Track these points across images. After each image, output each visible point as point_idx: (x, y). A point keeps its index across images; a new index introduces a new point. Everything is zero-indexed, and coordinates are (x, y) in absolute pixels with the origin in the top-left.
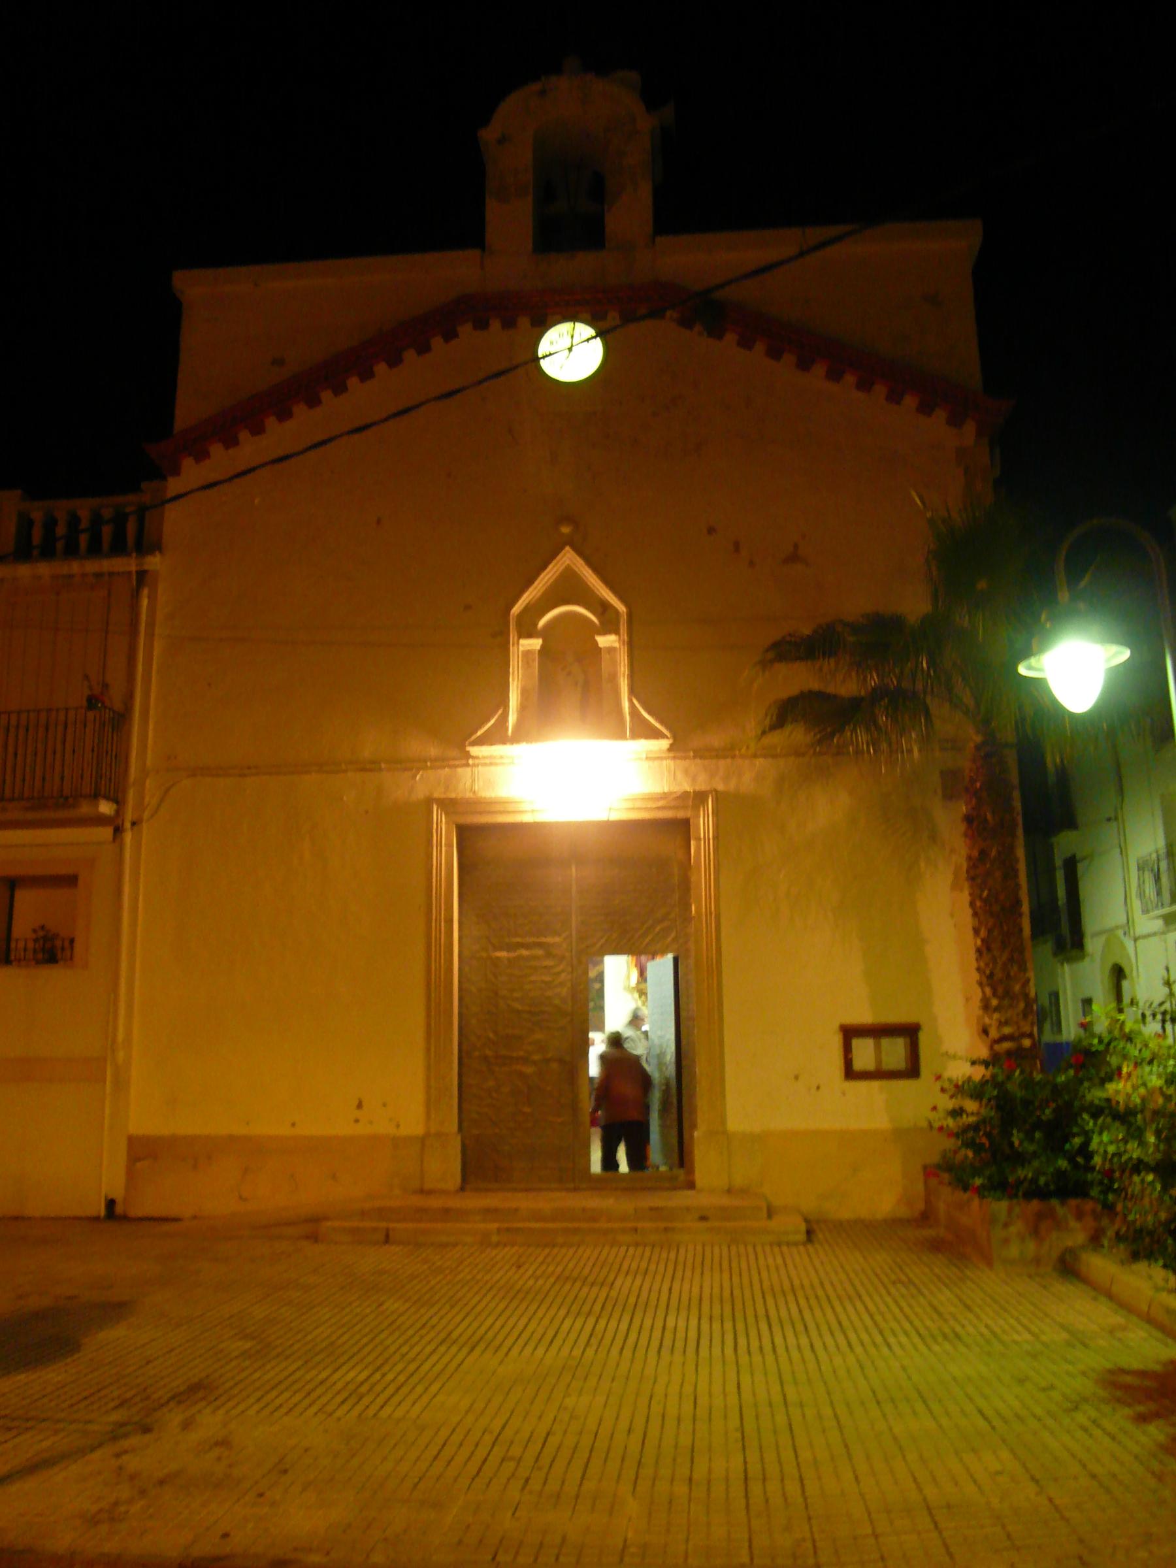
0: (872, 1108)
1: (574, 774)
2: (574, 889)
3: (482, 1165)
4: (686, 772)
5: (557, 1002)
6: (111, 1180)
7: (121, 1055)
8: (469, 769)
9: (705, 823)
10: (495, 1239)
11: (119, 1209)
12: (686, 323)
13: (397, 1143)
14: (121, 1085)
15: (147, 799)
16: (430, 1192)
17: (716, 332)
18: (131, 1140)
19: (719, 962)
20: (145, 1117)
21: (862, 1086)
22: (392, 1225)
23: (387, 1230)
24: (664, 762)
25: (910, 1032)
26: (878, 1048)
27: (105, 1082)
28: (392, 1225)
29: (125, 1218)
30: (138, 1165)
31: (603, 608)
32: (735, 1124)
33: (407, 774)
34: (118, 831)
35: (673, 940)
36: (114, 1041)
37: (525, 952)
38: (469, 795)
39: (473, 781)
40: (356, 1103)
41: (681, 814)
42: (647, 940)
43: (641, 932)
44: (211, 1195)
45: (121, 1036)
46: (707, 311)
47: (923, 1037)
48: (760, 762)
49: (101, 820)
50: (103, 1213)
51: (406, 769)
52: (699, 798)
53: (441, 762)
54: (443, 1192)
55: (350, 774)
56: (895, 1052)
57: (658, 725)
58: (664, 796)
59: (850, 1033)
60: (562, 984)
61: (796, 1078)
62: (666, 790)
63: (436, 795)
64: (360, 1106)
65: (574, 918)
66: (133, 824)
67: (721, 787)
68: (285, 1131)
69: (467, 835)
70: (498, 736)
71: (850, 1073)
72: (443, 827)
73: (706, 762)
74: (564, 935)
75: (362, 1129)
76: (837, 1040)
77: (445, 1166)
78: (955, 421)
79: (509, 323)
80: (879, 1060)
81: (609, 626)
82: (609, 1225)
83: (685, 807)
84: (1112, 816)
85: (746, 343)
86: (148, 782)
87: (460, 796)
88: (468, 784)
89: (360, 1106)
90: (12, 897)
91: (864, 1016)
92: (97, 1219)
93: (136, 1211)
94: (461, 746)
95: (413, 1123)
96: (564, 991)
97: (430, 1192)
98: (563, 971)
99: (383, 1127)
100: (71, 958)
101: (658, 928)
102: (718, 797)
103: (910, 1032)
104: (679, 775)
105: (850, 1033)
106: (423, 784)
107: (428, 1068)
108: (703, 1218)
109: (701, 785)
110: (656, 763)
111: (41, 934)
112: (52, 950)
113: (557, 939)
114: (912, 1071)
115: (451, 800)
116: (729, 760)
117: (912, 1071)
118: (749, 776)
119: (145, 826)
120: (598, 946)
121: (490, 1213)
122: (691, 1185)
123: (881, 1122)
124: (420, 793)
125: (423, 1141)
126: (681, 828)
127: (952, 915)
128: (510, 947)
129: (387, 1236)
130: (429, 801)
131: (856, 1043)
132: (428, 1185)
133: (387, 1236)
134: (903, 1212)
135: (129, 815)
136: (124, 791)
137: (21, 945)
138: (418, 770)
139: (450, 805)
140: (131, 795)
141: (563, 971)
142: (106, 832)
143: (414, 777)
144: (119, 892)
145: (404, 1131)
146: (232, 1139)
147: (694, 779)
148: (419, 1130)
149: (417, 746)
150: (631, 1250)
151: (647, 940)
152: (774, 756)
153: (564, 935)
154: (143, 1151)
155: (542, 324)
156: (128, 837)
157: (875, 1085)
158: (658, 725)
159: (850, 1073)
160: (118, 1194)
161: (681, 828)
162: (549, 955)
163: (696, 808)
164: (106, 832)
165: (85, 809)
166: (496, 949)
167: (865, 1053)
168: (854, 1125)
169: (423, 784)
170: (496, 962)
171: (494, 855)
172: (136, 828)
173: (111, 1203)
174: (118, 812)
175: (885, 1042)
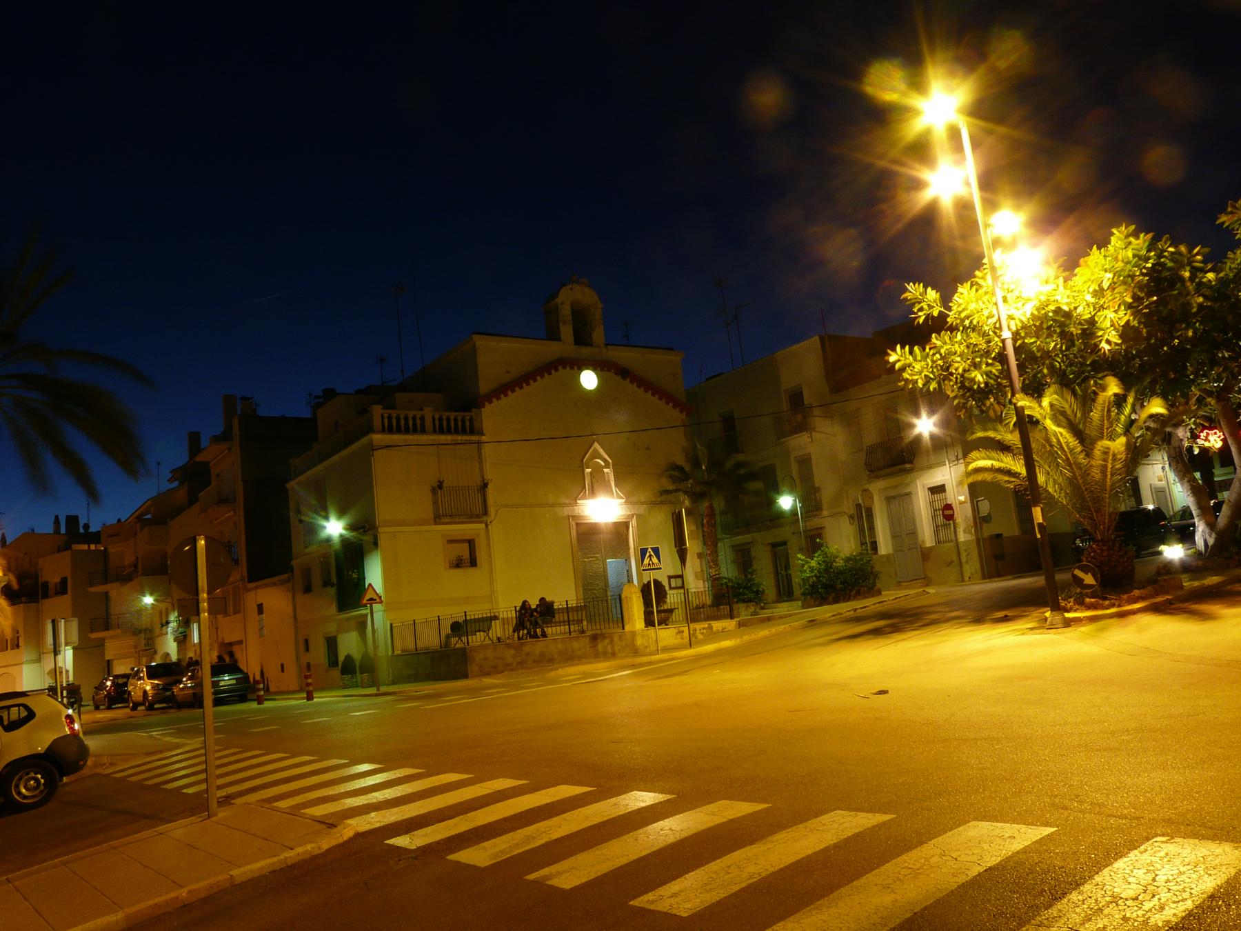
1: (604, 508)
9: (634, 523)
12: (617, 374)
17: (624, 378)
31: (604, 460)
46: (624, 372)
53: (570, 505)
57: (177, 740)
70: (585, 498)
72: (573, 523)
78: (681, 412)
79: (572, 368)
81: (607, 466)
84: (564, 594)
85: (632, 382)
94: (576, 499)
139: (574, 517)
149: (563, 500)
155: (580, 370)
158: (177, 740)
161: (626, 525)
169: (566, 511)
171: (587, 534)
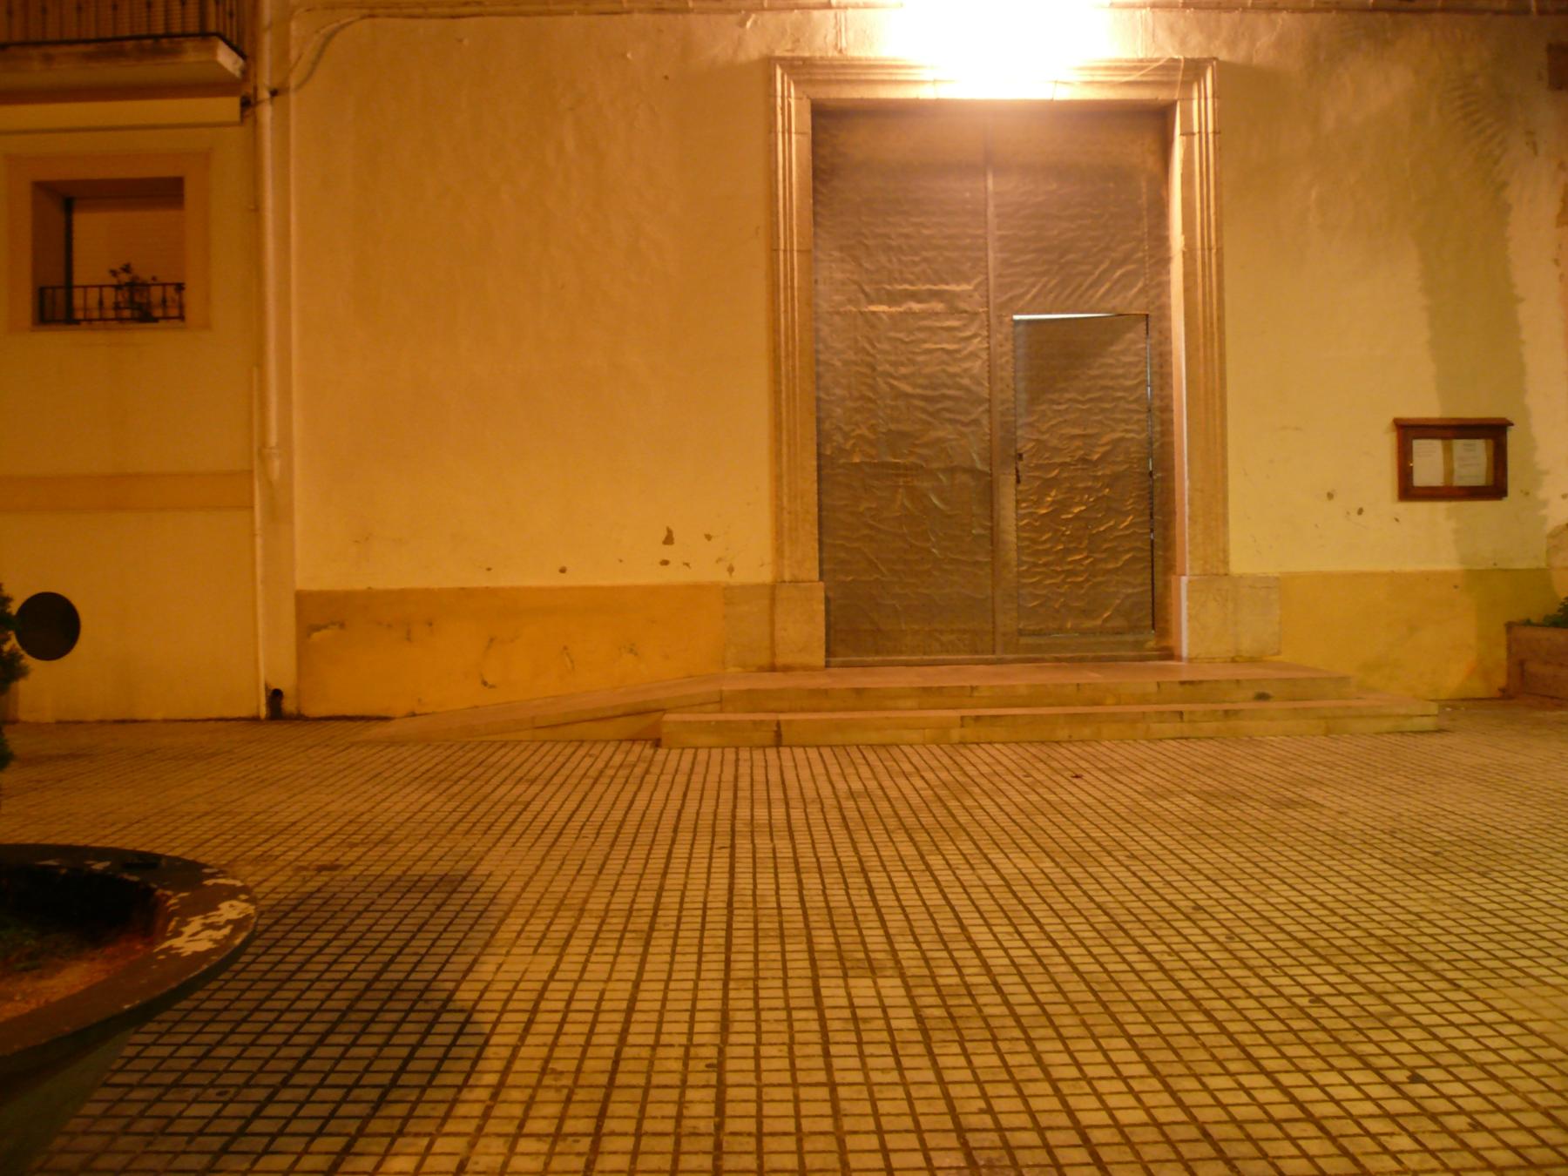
0: (1434, 540)
2: (991, 210)
3: (853, 630)
4: (1172, 30)
5: (966, 381)
6: (275, 661)
7: (276, 464)
8: (830, 13)
9: (1199, 110)
10: (956, 735)
11: (289, 706)
13: (730, 595)
14: (279, 514)
15: (294, 54)
16: (787, 669)
18: (302, 598)
19: (1221, 319)
20: (318, 569)
21: (1422, 508)
22: (782, 717)
23: (778, 724)
24: (1138, 13)
25: (1494, 432)
26: (1448, 451)
27: (252, 507)
28: (782, 717)
29: (300, 718)
30: (316, 636)
32: (1242, 562)
33: (732, 18)
34: (248, 104)
35: (1141, 291)
36: (264, 444)
37: (916, 307)
38: (832, 53)
39: (838, 33)
40: (663, 534)
41: (1162, 95)
42: (1102, 290)
43: (1090, 279)
44: (436, 680)
45: (273, 439)
47: (1511, 435)
48: (1283, 18)
49: (220, 86)
50: (263, 712)
51: (730, 11)
52: (1194, 69)
54: (807, 668)
55: (636, 16)
56: (1472, 460)
58: (1139, 65)
59: (1408, 432)
60: (973, 355)
61: (1330, 496)
62: (1141, 55)
63: (778, 53)
64: (669, 540)
65: (991, 254)
66: (274, 93)
67: (1224, 56)
68: (548, 579)
69: (828, 119)
71: (1408, 491)
73: (1202, 15)
74: (976, 281)
75: (675, 576)
76: (1387, 445)
77: (802, 630)
80: (1449, 472)
82: (1118, 709)
83: (1169, 84)
86: (293, 25)
87: (818, 54)
88: (831, 38)
89: (669, 540)
90: (730, 1171)
91: (1429, 408)
92: (255, 719)
93: (314, 710)
95: (753, 562)
96: (977, 366)
97: (787, 669)
98: (975, 336)
99: (707, 572)
100: (181, 317)
101: (1118, 273)
102: (1225, 72)
103: (1494, 432)
104: (1161, 34)
105: (1408, 432)
106: (758, 36)
107: (777, 479)
108: (1262, 697)
109: (1196, 48)
110: (1126, 13)
111: (125, 278)
112: (144, 303)
113: (965, 287)
114: (1495, 489)
115: (804, 60)
116: (1236, 15)
117: (1495, 489)
118: (1265, 40)
119: (293, 97)
120: (1029, 297)
121: (929, 695)
122: (1169, 654)
123: (1447, 562)
124: (754, 49)
125: (772, 592)
126: (1155, 120)
127: (1556, 262)
128: (893, 299)
129: (778, 734)
130: (769, 63)
131: (1419, 445)
132: (781, 660)
133: (778, 734)
134: (1479, 688)
135: (266, 79)
136: (255, 40)
137: (93, 295)
138: (749, 11)
139: (802, 69)
140: (267, 41)
141: (975, 336)
142: (228, 107)
143: (742, 24)
144: (256, 209)
145: (741, 577)
146: (466, 593)
147: (1183, 43)
148: (766, 576)
150: (716, 753)
151: (1102, 290)
152: (1305, 11)
153: (976, 281)
154: (321, 616)
156: (266, 113)
157: (1442, 506)
159: (1408, 491)
160: (286, 684)
161: (1155, 120)
162: (954, 311)
163: (1186, 85)
164: (228, 107)
165: (191, 58)
166: (871, 302)
167: (1429, 462)
168: (1410, 567)
169: (758, 36)
170: (871, 320)
172: (277, 99)
173: (275, 696)
174: (244, 72)
175: (1459, 445)
